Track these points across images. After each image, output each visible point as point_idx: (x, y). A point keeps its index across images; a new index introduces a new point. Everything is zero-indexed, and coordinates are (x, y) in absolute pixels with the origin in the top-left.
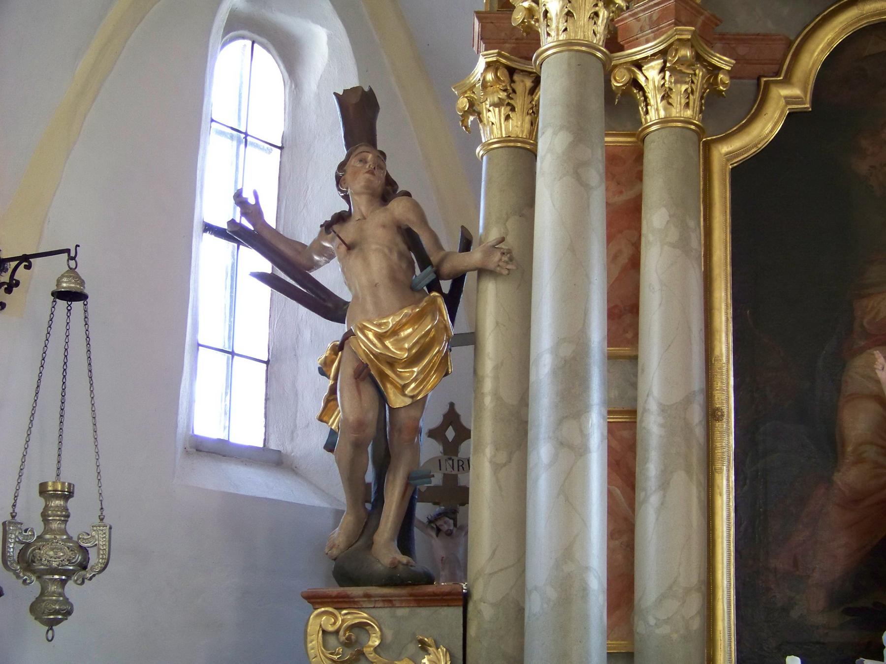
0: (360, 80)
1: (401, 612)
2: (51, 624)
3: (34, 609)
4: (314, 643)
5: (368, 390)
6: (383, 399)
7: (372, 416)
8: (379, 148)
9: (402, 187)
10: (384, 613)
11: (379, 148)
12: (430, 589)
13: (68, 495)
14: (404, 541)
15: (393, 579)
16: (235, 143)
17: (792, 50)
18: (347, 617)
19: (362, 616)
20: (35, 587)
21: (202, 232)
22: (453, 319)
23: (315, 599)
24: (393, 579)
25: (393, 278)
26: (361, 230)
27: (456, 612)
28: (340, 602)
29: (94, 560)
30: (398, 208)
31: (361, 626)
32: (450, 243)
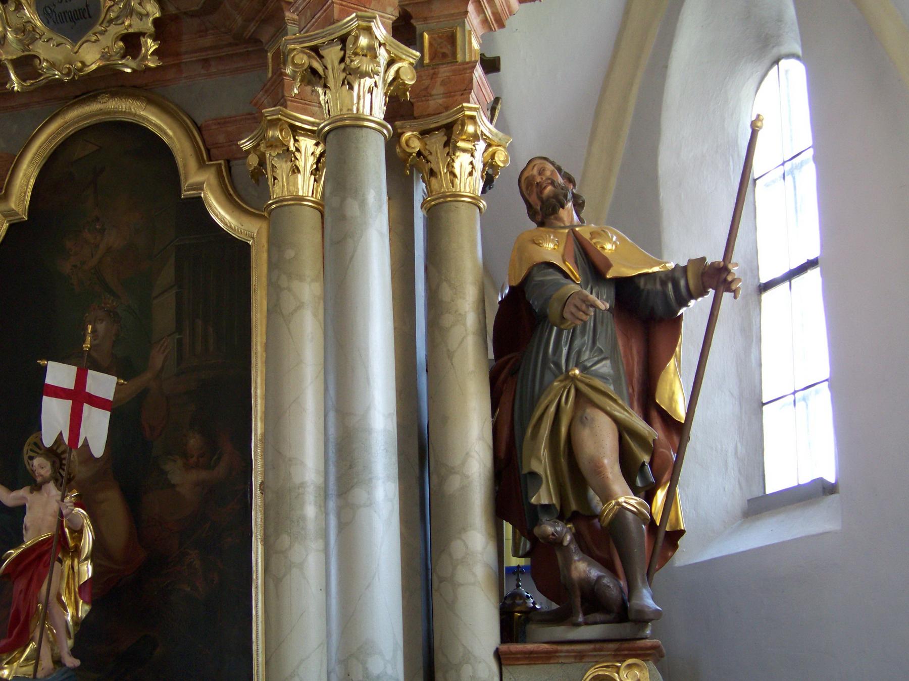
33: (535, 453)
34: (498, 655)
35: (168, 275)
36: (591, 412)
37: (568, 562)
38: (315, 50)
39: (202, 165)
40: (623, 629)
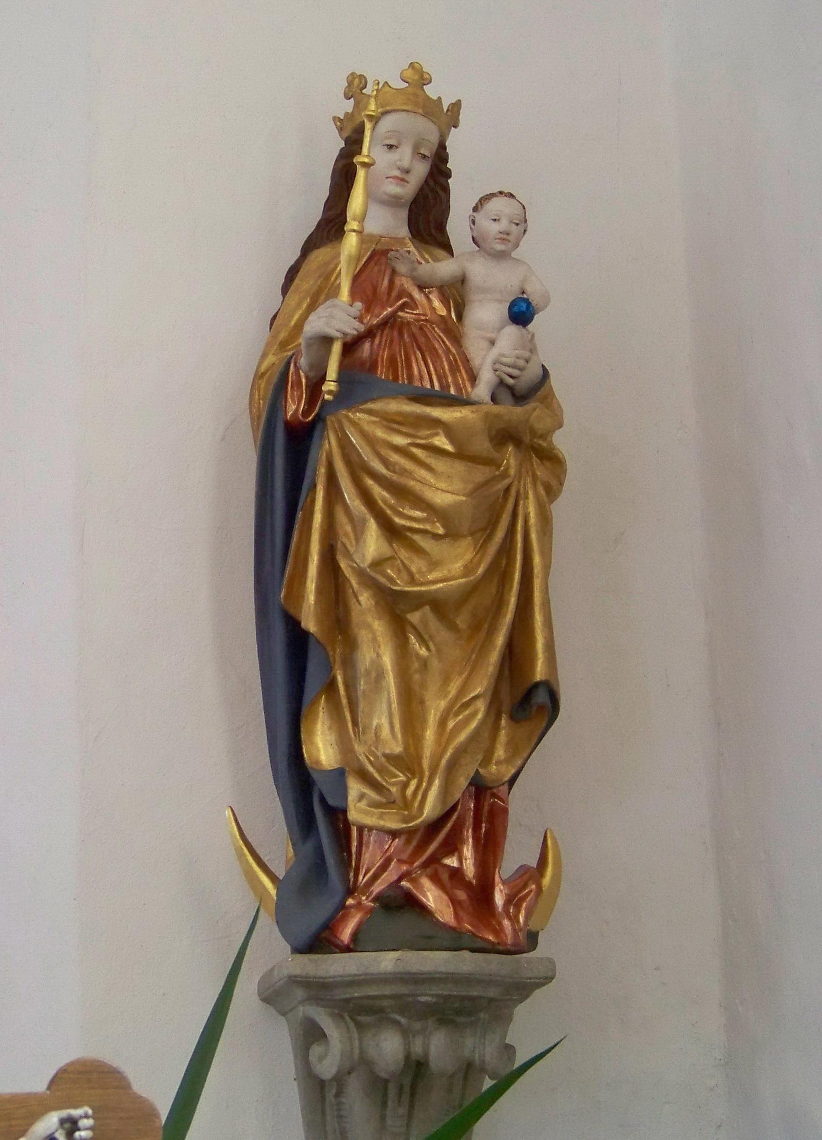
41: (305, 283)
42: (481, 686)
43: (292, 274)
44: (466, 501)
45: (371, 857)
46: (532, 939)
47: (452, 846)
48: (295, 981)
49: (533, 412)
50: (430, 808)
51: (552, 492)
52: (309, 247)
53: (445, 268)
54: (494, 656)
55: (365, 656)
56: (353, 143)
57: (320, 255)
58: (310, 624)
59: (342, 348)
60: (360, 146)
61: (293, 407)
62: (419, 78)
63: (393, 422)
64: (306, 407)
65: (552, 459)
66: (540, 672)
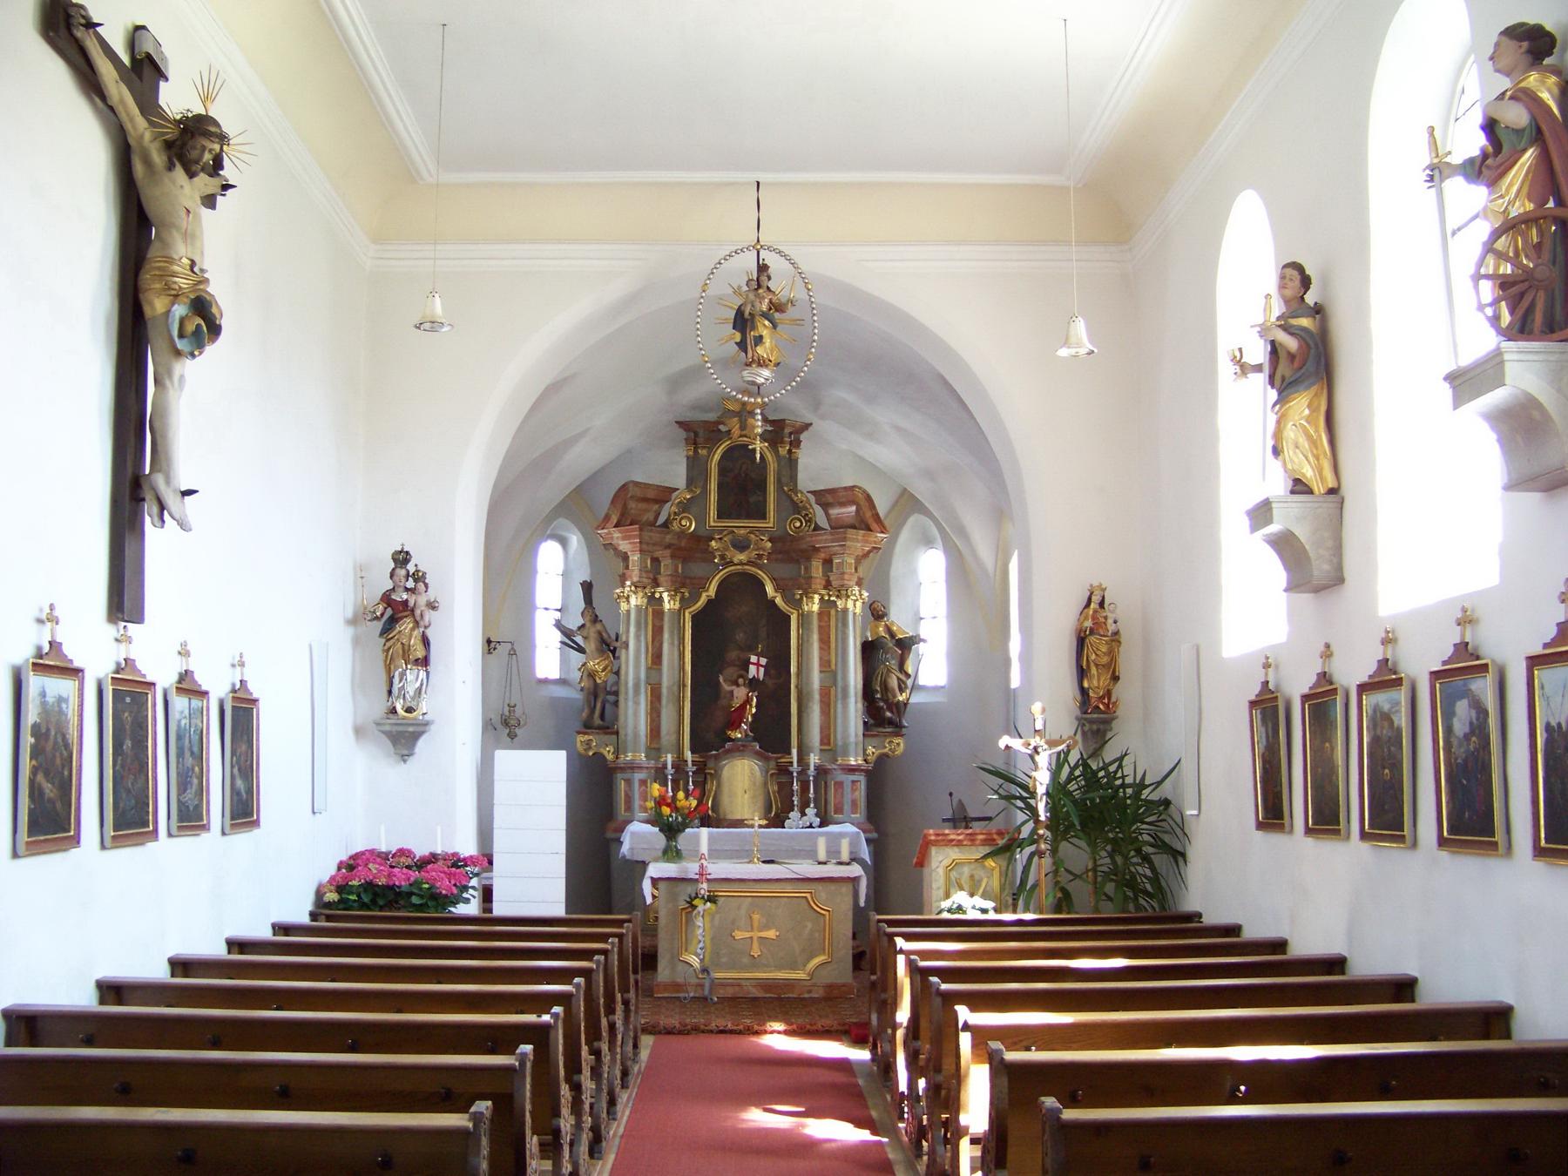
0: (592, 574)
1: (601, 736)
2: (512, 739)
3: (508, 735)
4: (579, 744)
5: (591, 678)
6: (595, 680)
7: (592, 686)
8: (575, 629)
9: (600, 618)
10: (597, 736)
11: (575, 629)
12: (609, 731)
13: (515, 706)
14: (602, 716)
15: (599, 728)
16: (424, 706)
17: (1184, 925)
18: (586, 737)
19: (591, 737)
20: (508, 731)
21: (593, 582)
22: (678, 489)
23: (579, 733)
24: (599, 728)
25: (597, 649)
26: (588, 633)
27: (615, 737)
28: (585, 733)
29: (522, 723)
30: (598, 626)
31: (591, 740)
32: (614, 637)
33: (876, 684)
34: (864, 735)
35: (764, 622)
36: (891, 674)
37: (884, 713)
38: (839, 591)
39: (776, 591)
40: (897, 730)
41: (1084, 615)
42: (1109, 676)
43: (1081, 613)
44: (208, 126)
45: (1093, 701)
46: (1115, 712)
47: (1104, 699)
48: (1082, 718)
49: (1117, 637)
50: (1101, 694)
51: (1119, 646)
52: (1084, 609)
53: (1105, 614)
54: (1111, 672)
55: (1092, 672)
56: (1092, 593)
57: (1086, 610)
58: (1085, 667)
59: (925, 890)
60: (994, 1063)
61: (1082, 635)
62: (1101, 585)
63: (1097, 639)
64: (1072, 834)
65: (1120, 642)
66: (1117, 674)
